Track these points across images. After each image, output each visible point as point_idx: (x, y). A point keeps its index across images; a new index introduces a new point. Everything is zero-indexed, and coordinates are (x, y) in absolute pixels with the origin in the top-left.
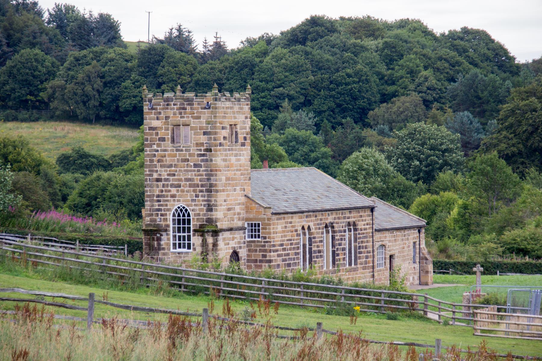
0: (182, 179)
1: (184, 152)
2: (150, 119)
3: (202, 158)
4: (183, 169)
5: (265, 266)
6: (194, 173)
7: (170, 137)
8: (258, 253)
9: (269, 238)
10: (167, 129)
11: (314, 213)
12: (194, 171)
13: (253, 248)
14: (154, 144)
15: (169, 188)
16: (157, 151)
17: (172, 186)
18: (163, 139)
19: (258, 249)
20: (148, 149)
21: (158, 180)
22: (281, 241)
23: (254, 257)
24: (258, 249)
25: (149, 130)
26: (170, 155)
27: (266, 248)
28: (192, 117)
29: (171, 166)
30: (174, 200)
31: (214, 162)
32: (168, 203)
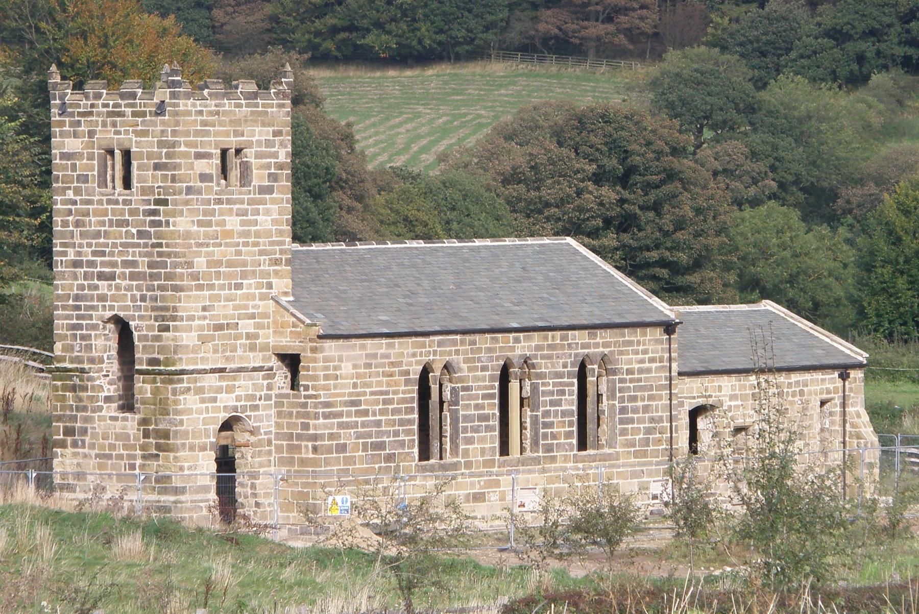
0: (117, 262)
1: (121, 206)
2: (62, 134)
3: (152, 218)
4: (118, 241)
5: (306, 447)
6: (137, 250)
7: (96, 173)
8: (294, 420)
9: (315, 388)
10: (91, 157)
11: (468, 338)
12: (138, 245)
13: (285, 409)
14: (69, 188)
15: (96, 281)
17: (101, 276)
18: (84, 179)
19: (295, 411)
20: (59, 198)
21: (76, 264)
22: (350, 394)
23: (288, 428)
24: (295, 411)
25: (61, 159)
27: (309, 409)
28: (133, 132)
29: (97, 235)
30: (105, 306)
31: (172, 228)
32: (94, 313)
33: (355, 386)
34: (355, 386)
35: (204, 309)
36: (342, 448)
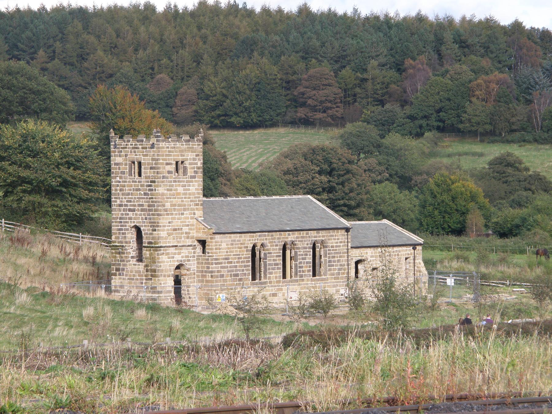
10: (126, 165)
11: (270, 234)
12: (144, 198)
16: (120, 182)
18: (123, 173)
21: (120, 205)
26: (128, 186)
29: (128, 194)
33: (227, 252)
34: (227, 252)
35: (169, 223)
36: (222, 276)
